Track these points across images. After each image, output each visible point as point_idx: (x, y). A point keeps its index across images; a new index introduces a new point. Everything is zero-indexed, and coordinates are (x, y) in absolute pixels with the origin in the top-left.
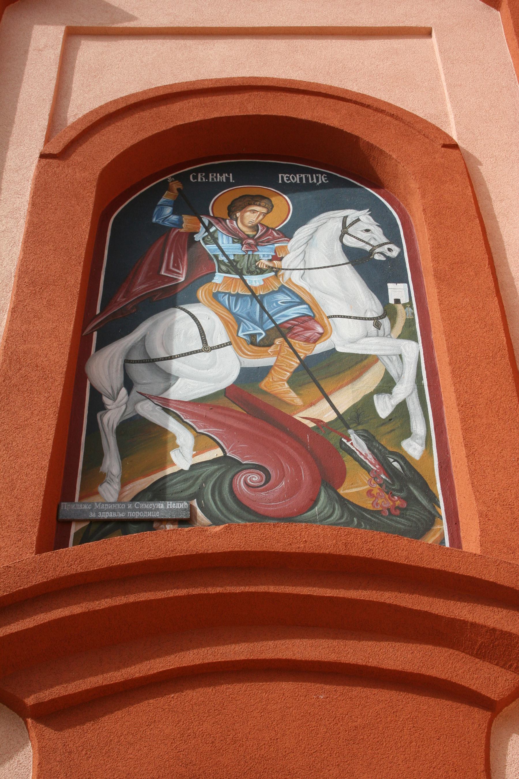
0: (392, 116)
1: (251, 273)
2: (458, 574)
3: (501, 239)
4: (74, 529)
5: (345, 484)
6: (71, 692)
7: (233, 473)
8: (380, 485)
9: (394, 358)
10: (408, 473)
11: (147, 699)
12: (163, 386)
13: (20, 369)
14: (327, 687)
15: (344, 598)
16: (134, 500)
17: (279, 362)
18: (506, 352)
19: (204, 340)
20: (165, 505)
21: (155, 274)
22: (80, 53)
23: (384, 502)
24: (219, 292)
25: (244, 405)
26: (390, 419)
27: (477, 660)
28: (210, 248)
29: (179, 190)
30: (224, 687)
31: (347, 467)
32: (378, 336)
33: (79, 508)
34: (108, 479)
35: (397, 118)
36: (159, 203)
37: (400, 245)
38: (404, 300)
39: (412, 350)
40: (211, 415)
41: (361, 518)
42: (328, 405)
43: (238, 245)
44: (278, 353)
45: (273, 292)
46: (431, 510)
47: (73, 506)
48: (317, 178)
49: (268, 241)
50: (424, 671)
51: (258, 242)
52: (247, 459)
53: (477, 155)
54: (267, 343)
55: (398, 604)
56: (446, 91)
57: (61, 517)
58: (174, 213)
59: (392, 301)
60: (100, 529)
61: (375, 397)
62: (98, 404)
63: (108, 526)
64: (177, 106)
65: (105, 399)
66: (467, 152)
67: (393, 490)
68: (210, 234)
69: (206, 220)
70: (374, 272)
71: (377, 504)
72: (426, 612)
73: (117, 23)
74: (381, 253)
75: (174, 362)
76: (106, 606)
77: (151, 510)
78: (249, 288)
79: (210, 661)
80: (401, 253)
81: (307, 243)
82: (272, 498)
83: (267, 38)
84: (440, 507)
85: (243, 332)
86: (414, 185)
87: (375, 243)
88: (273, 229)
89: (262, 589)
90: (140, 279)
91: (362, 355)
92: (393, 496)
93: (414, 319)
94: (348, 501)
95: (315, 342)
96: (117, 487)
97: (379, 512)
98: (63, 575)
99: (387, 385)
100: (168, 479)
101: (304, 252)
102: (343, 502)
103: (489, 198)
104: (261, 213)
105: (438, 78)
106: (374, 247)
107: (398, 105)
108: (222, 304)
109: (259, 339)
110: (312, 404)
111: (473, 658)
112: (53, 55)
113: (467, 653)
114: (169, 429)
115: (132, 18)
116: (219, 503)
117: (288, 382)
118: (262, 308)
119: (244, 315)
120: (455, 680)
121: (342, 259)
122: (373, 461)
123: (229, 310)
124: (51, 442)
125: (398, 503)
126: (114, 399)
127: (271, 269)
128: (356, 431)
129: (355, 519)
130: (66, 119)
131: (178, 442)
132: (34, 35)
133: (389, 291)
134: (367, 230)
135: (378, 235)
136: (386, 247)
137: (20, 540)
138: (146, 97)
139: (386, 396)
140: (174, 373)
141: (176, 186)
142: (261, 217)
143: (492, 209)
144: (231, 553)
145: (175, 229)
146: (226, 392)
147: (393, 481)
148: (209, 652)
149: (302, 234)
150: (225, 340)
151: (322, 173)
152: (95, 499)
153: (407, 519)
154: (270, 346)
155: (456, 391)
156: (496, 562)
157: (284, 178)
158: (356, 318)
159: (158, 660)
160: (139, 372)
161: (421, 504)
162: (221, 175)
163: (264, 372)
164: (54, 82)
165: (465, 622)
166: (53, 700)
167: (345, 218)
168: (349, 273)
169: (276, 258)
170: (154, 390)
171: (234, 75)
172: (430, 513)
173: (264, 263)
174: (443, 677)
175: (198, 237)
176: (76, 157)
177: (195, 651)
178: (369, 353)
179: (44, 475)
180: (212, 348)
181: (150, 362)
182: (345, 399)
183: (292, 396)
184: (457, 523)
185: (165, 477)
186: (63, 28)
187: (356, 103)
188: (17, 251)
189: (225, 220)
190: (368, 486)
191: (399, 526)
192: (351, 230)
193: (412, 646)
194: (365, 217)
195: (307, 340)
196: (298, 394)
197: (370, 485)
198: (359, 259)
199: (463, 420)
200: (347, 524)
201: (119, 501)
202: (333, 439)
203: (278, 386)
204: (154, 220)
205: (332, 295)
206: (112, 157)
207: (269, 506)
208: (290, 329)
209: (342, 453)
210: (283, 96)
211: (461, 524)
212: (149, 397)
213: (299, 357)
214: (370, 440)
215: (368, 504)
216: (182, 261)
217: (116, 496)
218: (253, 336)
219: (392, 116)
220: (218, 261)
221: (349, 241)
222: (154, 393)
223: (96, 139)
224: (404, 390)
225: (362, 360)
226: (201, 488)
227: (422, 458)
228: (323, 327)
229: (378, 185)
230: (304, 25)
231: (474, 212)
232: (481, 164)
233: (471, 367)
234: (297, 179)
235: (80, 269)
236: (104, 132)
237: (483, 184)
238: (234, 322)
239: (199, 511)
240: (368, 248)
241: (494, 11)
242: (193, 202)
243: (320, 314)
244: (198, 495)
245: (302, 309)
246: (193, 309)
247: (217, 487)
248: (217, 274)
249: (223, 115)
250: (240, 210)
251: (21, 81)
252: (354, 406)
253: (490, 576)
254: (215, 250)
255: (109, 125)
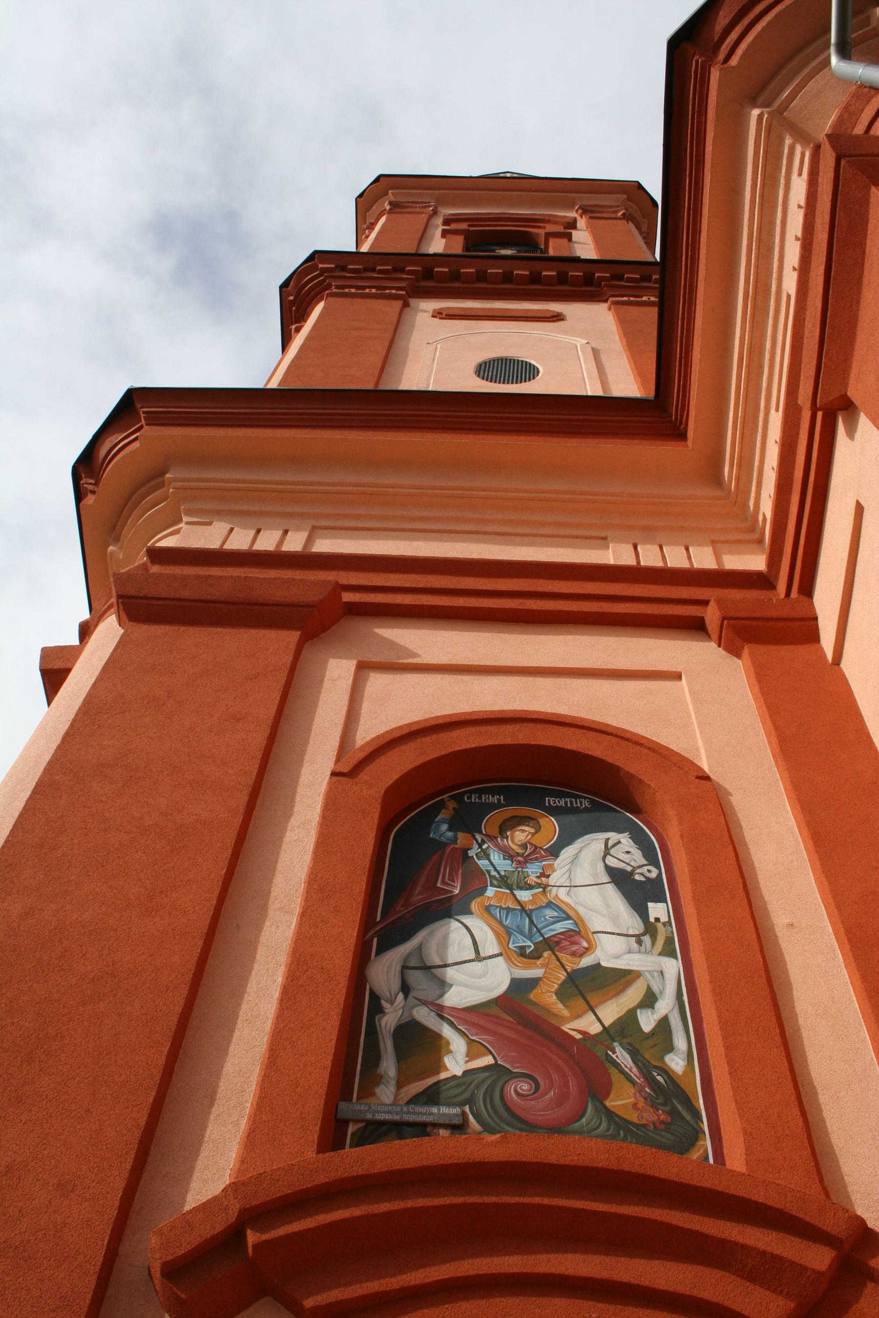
0: (650, 749)
1: (520, 888)
2: (727, 1194)
3: (752, 864)
4: (351, 1128)
5: (612, 1096)
6: (348, 1297)
7: (504, 1081)
8: (645, 1099)
9: (656, 974)
10: (671, 1087)
11: (421, 1308)
12: (438, 992)
13: (307, 971)
14: (600, 1305)
15: (616, 1213)
16: (409, 1103)
17: (547, 974)
18: (763, 972)
19: (477, 951)
20: (439, 1110)
21: (431, 885)
22: (369, 684)
23: (649, 1116)
24: (490, 905)
25: (512, 1015)
26: (653, 1033)
27: (748, 1284)
28: (483, 863)
29: (454, 808)
30: (497, 1300)
31: (613, 1079)
32: (640, 952)
33: (355, 1107)
34: (384, 1080)
35: (654, 751)
36: (437, 820)
37: (658, 866)
38: (664, 919)
39: (673, 967)
40: (482, 1022)
41: (627, 1131)
42: (594, 1017)
43: (509, 862)
44: (546, 965)
45: (541, 907)
46: (695, 1125)
47: (351, 1106)
48: (581, 802)
49: (536, 859)
50: (696, 1293)
51: (527, 860)
52: (517, 1067)
53: (727, 786)
54: (535, 956)
55: (669, 1222)
56: (696, 728)
57: (339, 1116)
58: (449, 829)
59: (652, 920)
60: (376, 1131)
61: (638, 1011)
62: (376, 1008)
63: (384, 1128)
64: (455, 733)
65: (383, 1003)
66: (718, 784)
67: (658, 1103)
68: (483, 850)
69: (479, 837)
70: (636, 892)
71: (642, 1118)
72: (697, 1231)
73: (406, 658)
74: (641, 874)
75: (449, 969)
76: (385, 1209)
77: (425, 1114)
78: (519, 902)
79: (484, 1272)
80: (660, 875)
81: (572, 862)
82: (541, 1109)
83: (535, 676)
84: (702, 1122)
85: (513, 943)
86: (671, 812)
87: (635, 865)
88: (541, 848)
89: (536, 1200)
90: (418, 889)
91: (625, 970)
92: (657, 1110)
93: (673, 938)
94: (614, 1113)
95: (581, 956)
96: (393, 1089)
97: (644, 1126)
98: (344, 1176)
99: (649, 1000)
100: (441, 1084)
101: (570, 870)
102: (610, 1114)
103: (741, 827)
104: (530, 833)
105: (689, 716)
106: (634, 868)
107: (654, 739)
108: (494, 917)
109: (528, 951)
110: (579, 1016)
111: (744, 1281)
112: (346, 684)
113: (737, 1276)
114: (443, 1035)
115: (416, 655)
116: (490, 1110)
117: (556, 994)
118: (531, 921)
119: (514, 928)
120: (726, 1303)
121: (605, 878)
122: (637, 1074)
123: (500, 922)
124: (333, 1042)
125: (662, 1117)
126: (392, 1002)
127: (539, 885)
128: (621, 1045)
129: (621, 1132)
130: (354, 741)
131: (452, 1047)
132: (329, 667)
133: (650, 910)
134: (626, 852)
135: (637, 857)
136: (646, 868)
137: (302, 1138)
138: (427, 725)
139: (649, 1012)
140: (448, 980)
141: (452, 805)
142: (530, 836)
143: (743, 837)
144: (507, 1162)
145: (450, 844)
146: (499, 1001)
147: (657, 1095)
148: (484, 1263)
149: (567, 853)
150: (496, 951)
151: (585, 798)
152: (372, 1100)
153: (673, 1134)
154: (538, 958)
155: (717, 1009)
156: (764, 1182)
157: (550, 801)
158: (619, 934)
159: (433, 1268)
160: (416, 978)
161: (683, 1118)
162: (493, 796)
163: (533, 983)
164: (346, 708)
165: (735, 1243)
166: (330, 1303)
167: (607, 840)
168: (611, 891)
169: (543, 875)
170: (430, 996)
171: (505, 708)
172: (694, 1128)
173: (532, 879)
174: (715, 1299)
175: (471, 853)
176: (364, 776)
177: (470, 1261)
178: (632, 968)
179: (326, 1075)
180: (485, 958)
181: (427, 968)
182: (611, 1012)
183: (559, 1008)
184: (720, 1140)
185: (439, 1082)
186: (355, 662)
187: (616, 736)
188: (308, 858)
189: (496, 838)
190: (633, 1099)
191: (664, 1140)
192: (612, 851)
193: (683, 1266)
194: (625, 839)
195: (574, 954)
196: (565, 1006)
197: (635, 1097)
198: (620, 879)
199: (725, 1037)
200: (614, 1137)
201: (395, 1103)
202: (599, 1051)
203: (547, 997)
204: (431, 835)
205: (597, 912)
206: (395, 777)
207: (539, 1115)
208: (558, 943)
209: (608, 1065)
210: (550, 728)
211: (724, 1141)
212: (424, 1003)
213: (566, 970)
214: (634, 1053)
215: (633, 1117)
216: (457, 874)
217: (392, 1098)
218: (522, 948)
219: (650, 749)
220: (491, 876)
221: (611, 862)
222: (430, 999)
223: (382, 761)
224: (665, 1005)
225: (625, 976)
226: (473, 1094)
227: (685, 1072)
228: (589, 942)
229: (636, 810)
230: (568, 666)
231: (726, 839)
232: (731, 795)
233: (730, 986)
234: (562, 803)
235: (365, 878)
236: (389, 754)
237: (734, 813)
238: (504, 934)
239: (471, 1116)
240: (629, 869)
241: (736, 660)
242: (468, 821)
243: (586, 930)
244: (470, 1101)
245: (567, 925)
246: (468, 920)
247: (489, 1093)
248: (489, 888)
249: (497, 743)
250: (510, 830)
251: (316, 706)
252: (619, 1020)
253: (760, 1196)
254: (487, 866)
255: (394, 748)
